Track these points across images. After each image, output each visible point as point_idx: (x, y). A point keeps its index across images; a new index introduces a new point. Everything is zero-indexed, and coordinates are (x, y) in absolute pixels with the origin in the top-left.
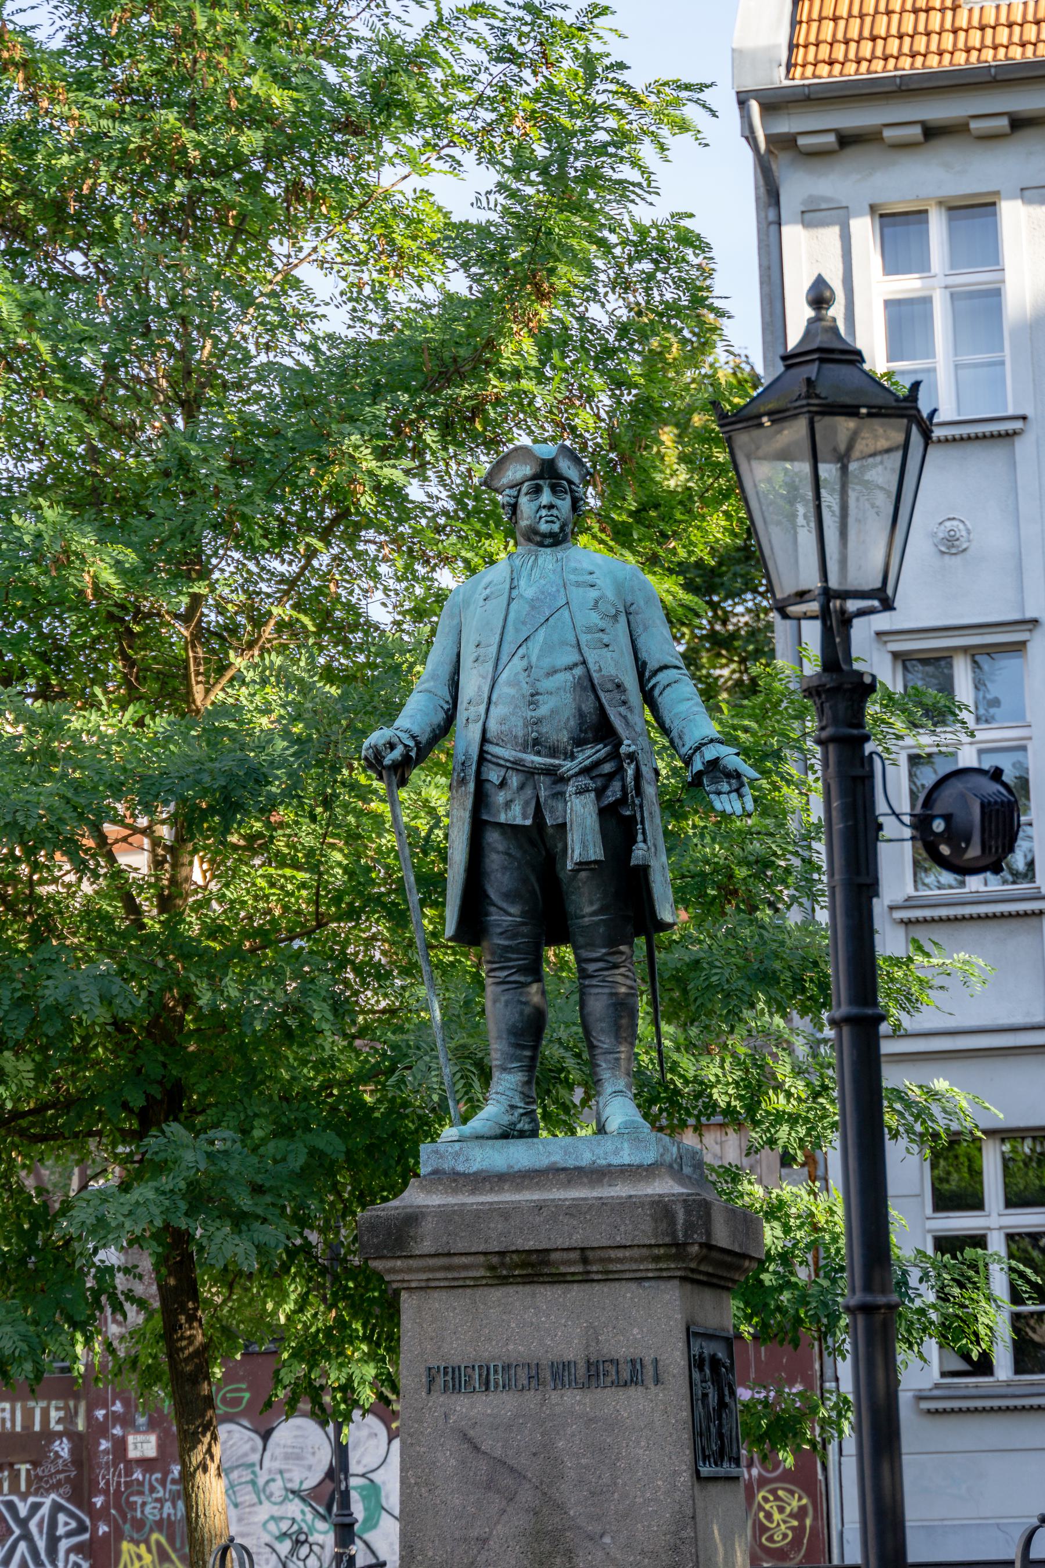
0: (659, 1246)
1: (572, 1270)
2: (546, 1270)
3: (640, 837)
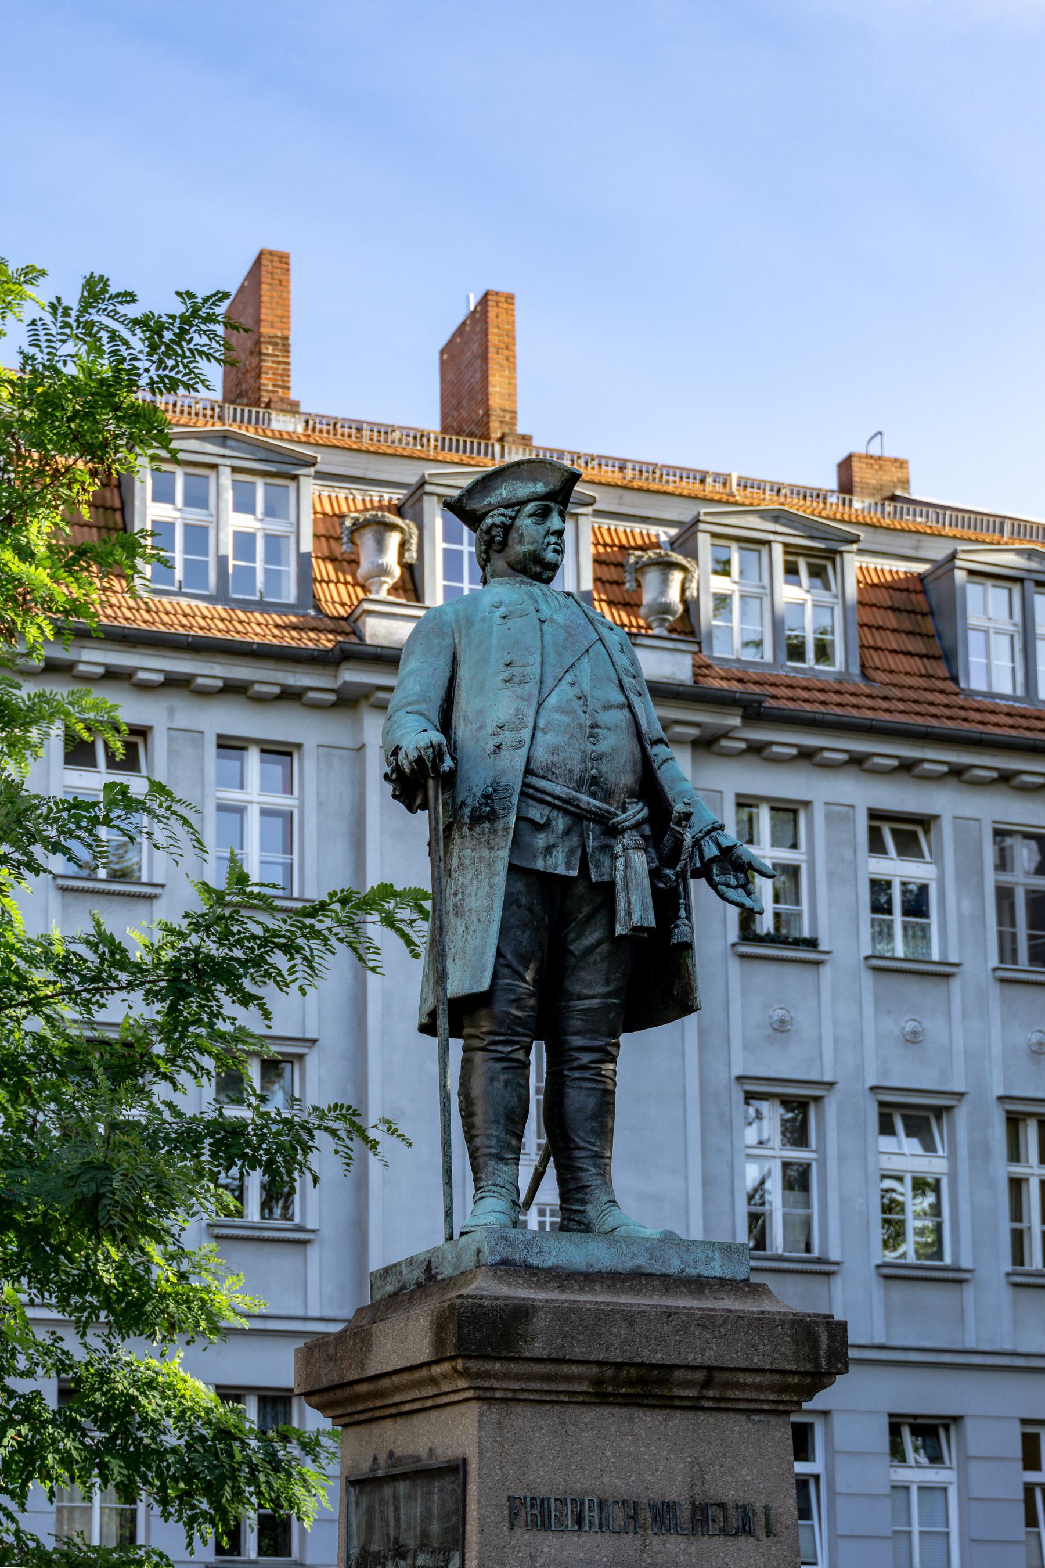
0: (793, 1373)
1: (686, 1393)
2: (657, 1391)
3: (683, 913)
